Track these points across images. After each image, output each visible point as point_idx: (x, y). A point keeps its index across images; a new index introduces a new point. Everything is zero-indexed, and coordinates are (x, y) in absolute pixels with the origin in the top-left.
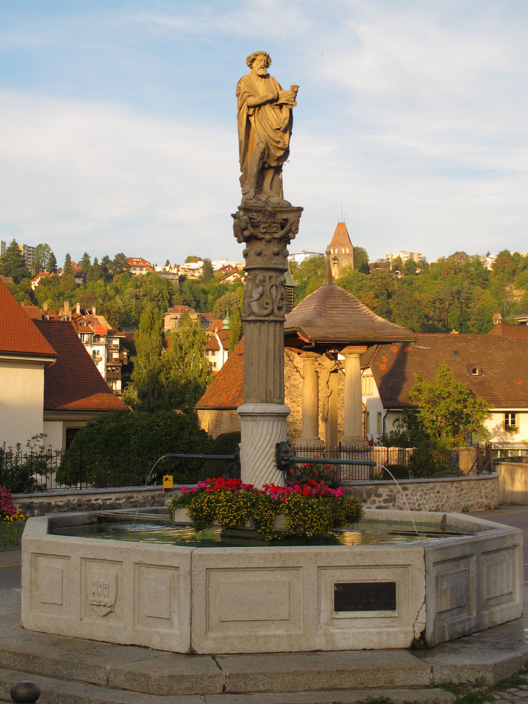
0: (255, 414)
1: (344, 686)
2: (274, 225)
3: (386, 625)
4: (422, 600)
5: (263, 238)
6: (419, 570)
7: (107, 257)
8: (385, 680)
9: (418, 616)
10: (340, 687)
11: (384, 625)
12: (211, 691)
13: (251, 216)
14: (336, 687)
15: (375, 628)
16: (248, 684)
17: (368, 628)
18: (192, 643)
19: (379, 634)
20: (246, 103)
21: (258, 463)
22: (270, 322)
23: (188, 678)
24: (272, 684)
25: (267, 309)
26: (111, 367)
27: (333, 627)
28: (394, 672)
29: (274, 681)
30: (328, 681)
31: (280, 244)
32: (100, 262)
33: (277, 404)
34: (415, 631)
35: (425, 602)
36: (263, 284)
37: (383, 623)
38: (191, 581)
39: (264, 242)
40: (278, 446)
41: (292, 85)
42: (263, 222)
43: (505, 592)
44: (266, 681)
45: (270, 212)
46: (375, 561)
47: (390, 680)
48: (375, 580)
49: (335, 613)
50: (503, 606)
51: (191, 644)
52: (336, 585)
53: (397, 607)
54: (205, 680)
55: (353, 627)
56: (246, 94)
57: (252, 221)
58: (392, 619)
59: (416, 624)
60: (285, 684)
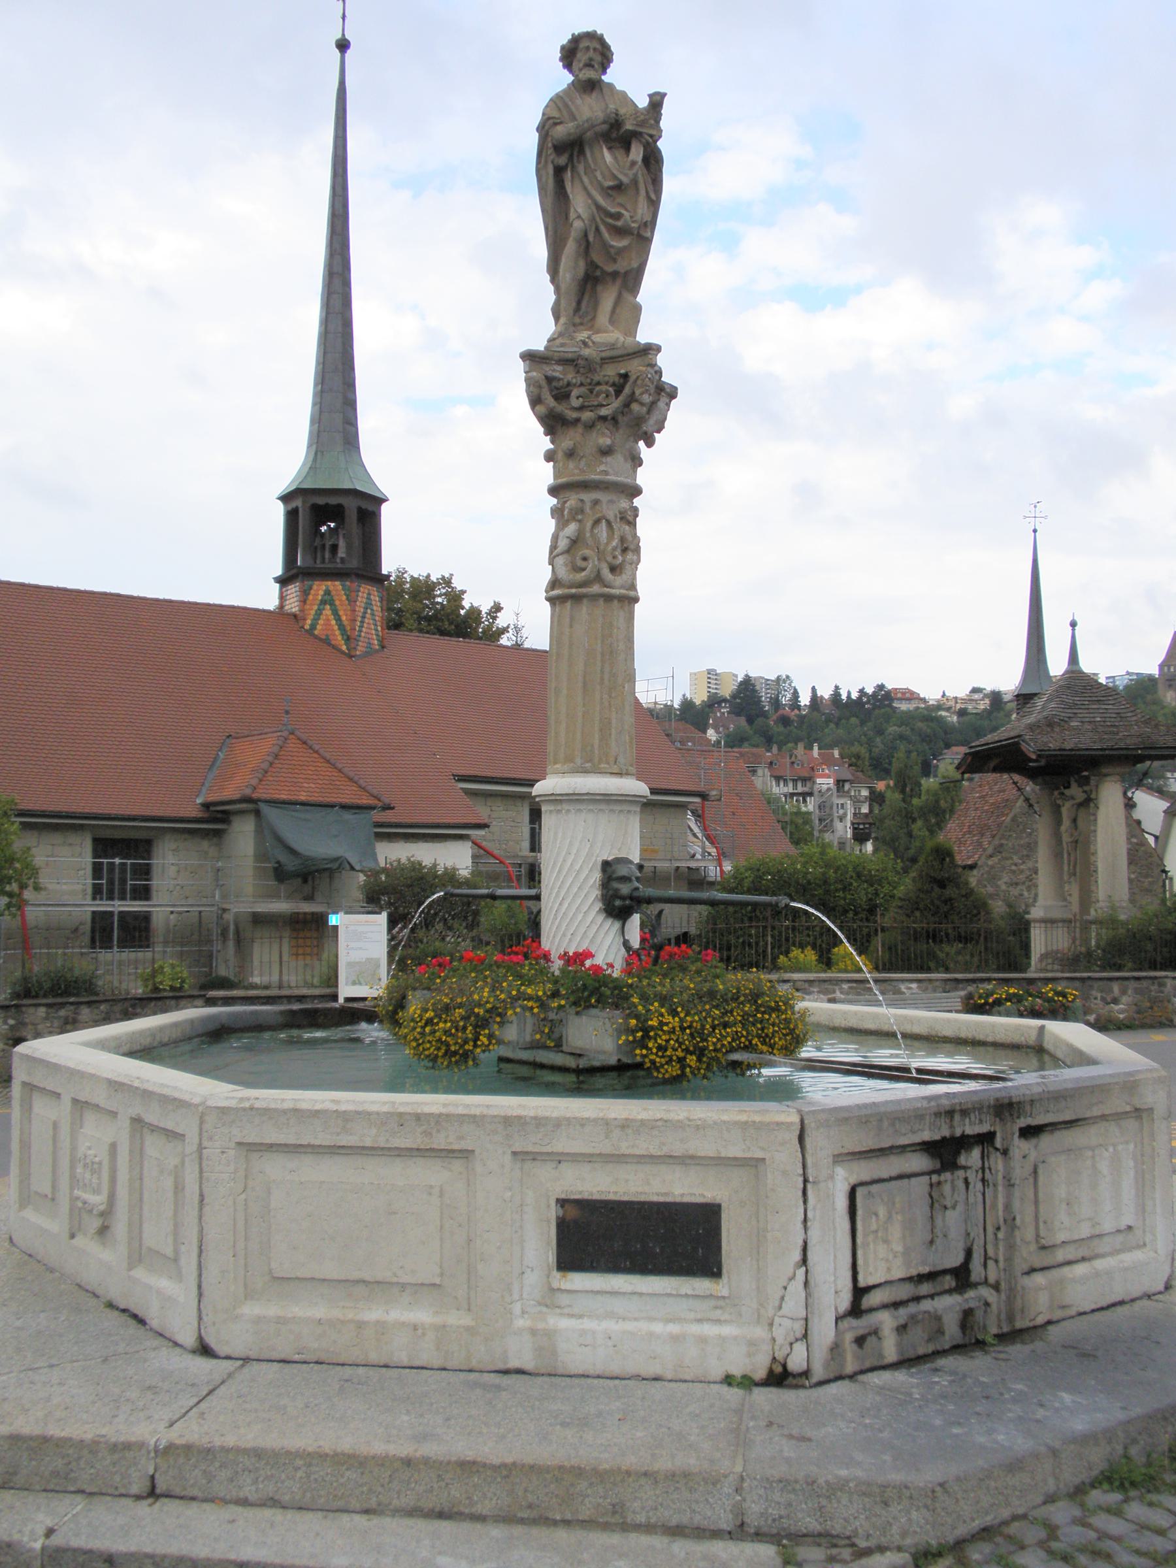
0: (558, 798)
1: (479, 1509)
2: (598, 388)
3: (699, 1317)
4: (797, 1256)
5: (578, 420)
6: (785, 1173)
7: (864, 688)
8: (599, 1505)
9: (782, 1298)
10: (467, 1511)
11: (692, 1315)
12: (116, 1488)
13: (550, 373)
14: (455, 1510)
15: (669, 1321)
16: (215, 1476)
17: (651, 1319)
18: (202, 1327)
19: (676, 1339)
20: (549, 139)
21: (566, 905)
22: (594, 598)
23: (57, 1445)
24: (279, 1485)
25: (584, 569)
26: (859, 824)
27: (558, 1311)
28: (623, 1481)
29: (283, 1476)
30: (431, 1490)
31: (617, 429)
32: (854, 696)
33: (608, 775)
34: (774, 1340)
35: (804, 1261)
36: (580, 517)
37: (690, 1310)
38: (201, 1171)
39: (580, 429)
40: (606, 865)
41: (651, 92)
42: (575, 385)
43: (1108, 1226)
44: (262, 1472)
45: (586, 359)
46: (664, 1144)
47: (614, 1506)
48: (666, 1194)
49: (557, 1275)
50: (1099, 1264)
51: (199, 1330)
52: (562, 1203)
53: (724, 1271)
54: (100, 1455)
55: (610, 1315)
56: (551, 121)
57: (555, 384)
58: (713, 1303)
59: (777, 1320)
60: (314, 1486)
